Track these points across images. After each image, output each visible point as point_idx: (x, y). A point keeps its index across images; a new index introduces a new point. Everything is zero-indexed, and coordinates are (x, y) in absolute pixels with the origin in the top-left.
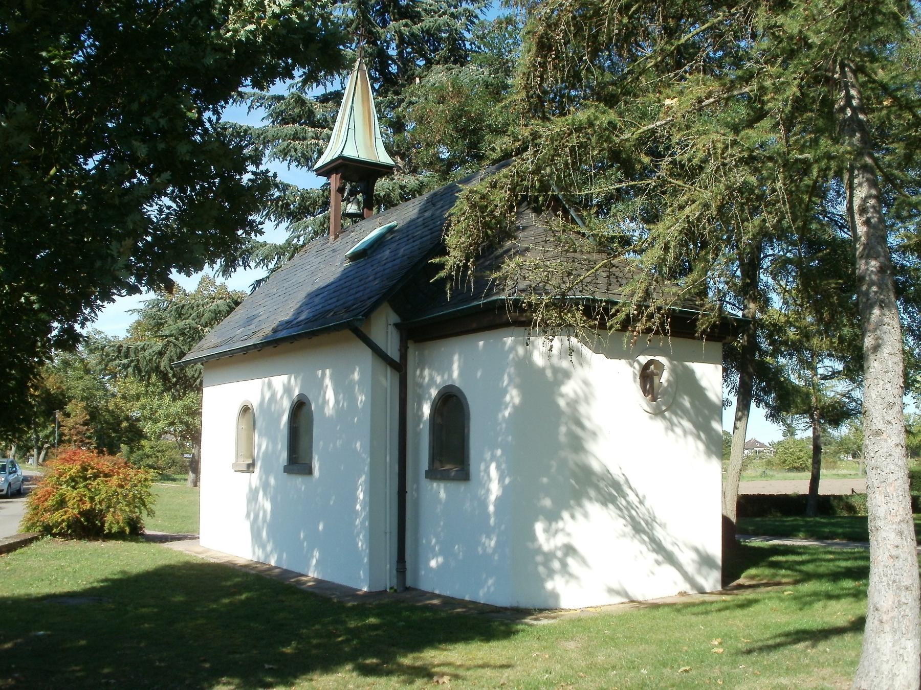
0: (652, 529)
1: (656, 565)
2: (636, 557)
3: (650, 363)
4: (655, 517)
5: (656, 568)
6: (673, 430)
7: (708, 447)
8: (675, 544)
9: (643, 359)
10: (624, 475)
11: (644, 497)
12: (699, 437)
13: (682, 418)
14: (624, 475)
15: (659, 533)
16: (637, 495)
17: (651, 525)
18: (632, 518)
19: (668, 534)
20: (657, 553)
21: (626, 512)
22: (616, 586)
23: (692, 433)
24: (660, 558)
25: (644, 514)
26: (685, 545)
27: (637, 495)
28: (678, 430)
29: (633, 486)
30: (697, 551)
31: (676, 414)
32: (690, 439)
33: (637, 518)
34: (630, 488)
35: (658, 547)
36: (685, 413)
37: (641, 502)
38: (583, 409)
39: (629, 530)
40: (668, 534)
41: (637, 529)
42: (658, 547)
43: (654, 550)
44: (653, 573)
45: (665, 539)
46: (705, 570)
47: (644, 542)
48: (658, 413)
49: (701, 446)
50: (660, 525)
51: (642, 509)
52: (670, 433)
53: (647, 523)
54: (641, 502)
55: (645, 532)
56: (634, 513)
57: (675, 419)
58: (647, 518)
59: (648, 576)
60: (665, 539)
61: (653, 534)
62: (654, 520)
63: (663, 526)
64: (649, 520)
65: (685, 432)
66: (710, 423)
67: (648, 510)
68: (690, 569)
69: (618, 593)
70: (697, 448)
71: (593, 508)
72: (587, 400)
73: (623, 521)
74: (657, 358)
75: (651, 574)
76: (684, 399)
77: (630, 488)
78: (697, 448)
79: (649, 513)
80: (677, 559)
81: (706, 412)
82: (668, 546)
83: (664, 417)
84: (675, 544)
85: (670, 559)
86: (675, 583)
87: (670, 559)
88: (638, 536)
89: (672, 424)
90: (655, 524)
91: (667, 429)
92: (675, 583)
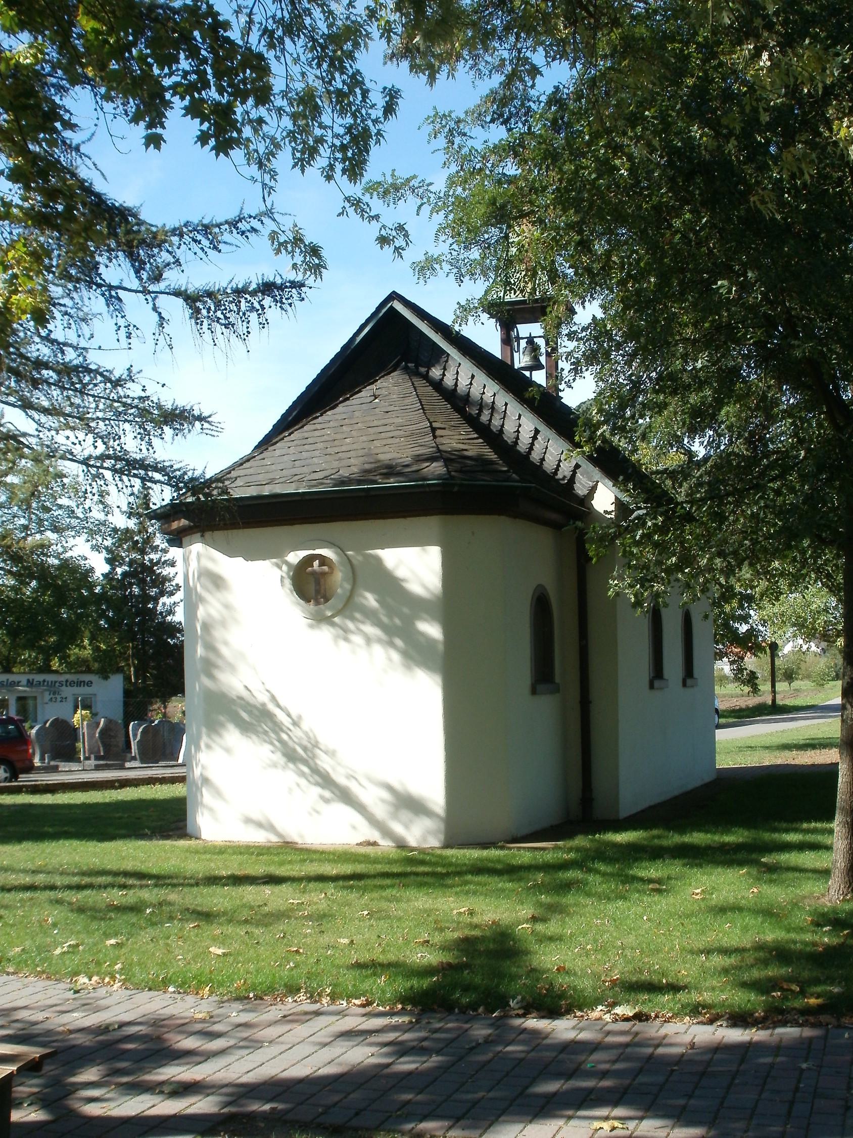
0: (314, 756)
1: (321, 802)
2: (290, 790)
3: (308, 560)
4: (317, 742)
5: (322, 806)
6: (346, 639)
7: (405, 654)
8: (350, 777)
9: (295, 557)
10: (268, 691)
11: (300, 717)
12: (392, 644)
13: (363, 623)
14: (268, 691)
15: (325, 763)
16: (289, 715)
17: (312, 752)
18: (281, 741)
19: (339, 764)
20: (323, 787)
21: (273, 735)
22: (256, 816)
23: (379, 641)
24: (327, 794)
25: (300, 739)
26: (370, 779)
27: (289, 715)
28: (357, 639)
29: (282, 703)
30: (390, 788)
31: (353, 619)
32: (378, 649)
33: (291, 743)
34: (279, 706)
35: (325, 781)
36: (370, 615)
37: (295, 724)
38: (218, 634)
39: (279, 758)
40: (339, 764)
41: (291, 756)
42: (325, 781)
43: (317, 784)
44: (317, 812)
45: (334, 770)
46: (405, 815)
47: (303, 774)
48: (320, 619)
49: (396, 656)
50: (326, 753)
51: (297, 733)
52: (342, 643)
53: (305, 749)
54: (295, 724)
55: (305, 762)
56: (285, 737)
57: (350, 625)
58: (305, 743)
59: (310, 814)
60: (334, 770)
61: (316, 764)
62: (316, 745)
63: (331, 754)
64: (309, 745)
65: (368, 640)
66: (414, 624)
67: (306, 734)
68: (380, 811)
69: (260, 825)
70: (390, 660)
71: (232, 736)
72: (223, 624)
73: (271, 747)
74: (318, 551)
75: (314, 814)
76: (366, 598)
77: (279, 706)
78: (390, 660)
79: (309, 738)
80: (357, 797)
81: (406, 610)
82: (341, 780)
83: (333, 625)
84: (350, 777)
85: (346, 797)
86: (354, 828)
87: (346, 797)
88: (291, 765)
89: (346, 630)
90: (318, 751)
91: (337, 637)
92: (354, 828)
